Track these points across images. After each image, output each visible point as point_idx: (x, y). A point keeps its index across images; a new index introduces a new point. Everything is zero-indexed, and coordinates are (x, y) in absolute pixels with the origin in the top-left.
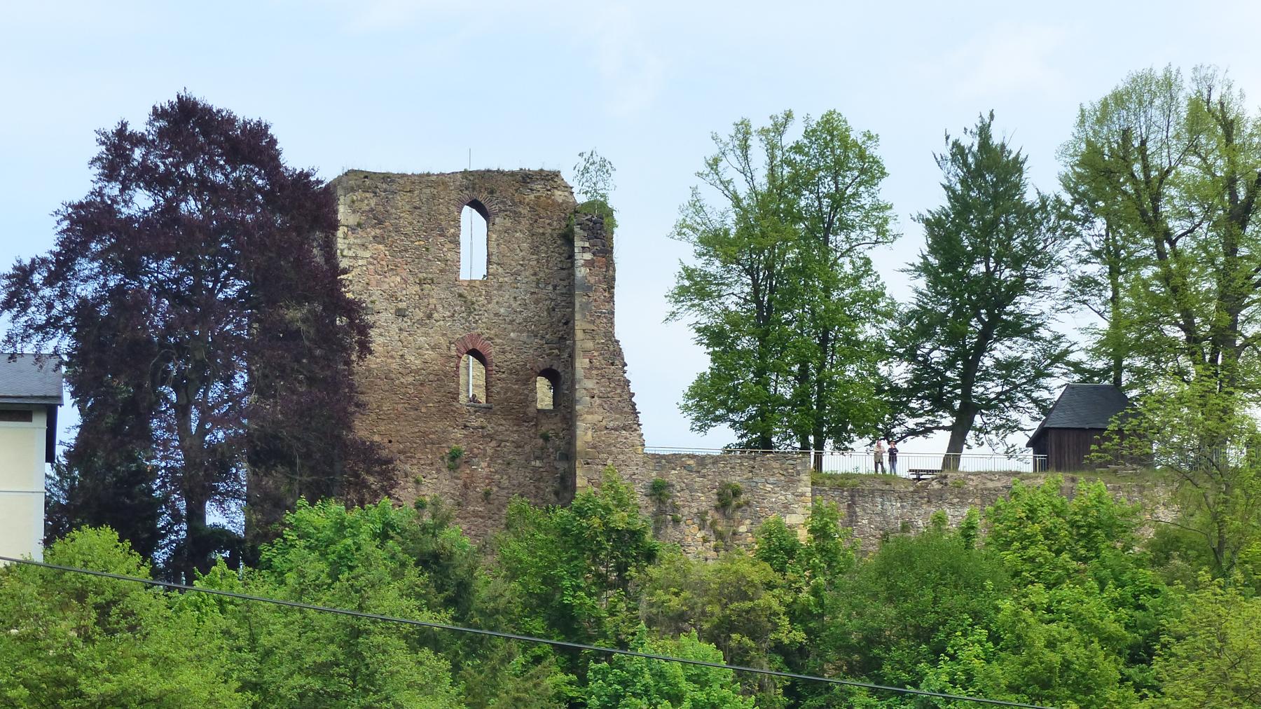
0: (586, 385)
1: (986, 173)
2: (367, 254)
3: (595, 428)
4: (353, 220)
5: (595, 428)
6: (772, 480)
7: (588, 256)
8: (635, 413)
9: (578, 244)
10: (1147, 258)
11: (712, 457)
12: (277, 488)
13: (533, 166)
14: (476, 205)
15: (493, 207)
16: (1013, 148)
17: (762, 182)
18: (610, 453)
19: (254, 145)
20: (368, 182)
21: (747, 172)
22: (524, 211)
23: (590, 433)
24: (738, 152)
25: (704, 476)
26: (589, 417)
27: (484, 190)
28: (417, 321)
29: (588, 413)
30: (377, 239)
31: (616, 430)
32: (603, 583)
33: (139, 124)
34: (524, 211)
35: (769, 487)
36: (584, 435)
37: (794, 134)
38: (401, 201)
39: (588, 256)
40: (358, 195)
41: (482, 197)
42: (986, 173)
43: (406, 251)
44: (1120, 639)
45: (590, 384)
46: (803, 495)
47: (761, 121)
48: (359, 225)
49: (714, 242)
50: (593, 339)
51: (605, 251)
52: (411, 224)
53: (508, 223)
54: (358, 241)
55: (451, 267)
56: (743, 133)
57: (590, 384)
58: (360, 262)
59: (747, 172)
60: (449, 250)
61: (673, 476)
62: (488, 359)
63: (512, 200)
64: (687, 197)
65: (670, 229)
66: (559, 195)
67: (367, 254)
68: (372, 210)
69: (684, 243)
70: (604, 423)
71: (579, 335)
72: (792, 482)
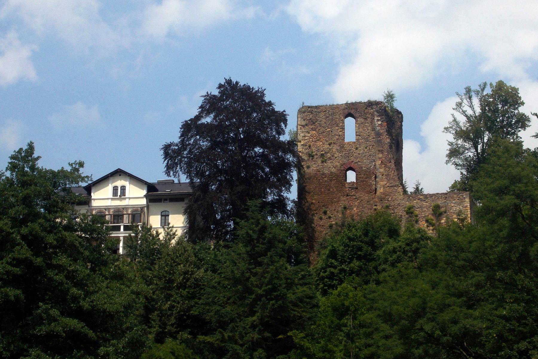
2: (309, 135)
3: (384, 187)
5: (384, 187)
6: (454, 202)
7: (380, 123)
9: (376, 118)
11: (430, 195)
12: (165, 216)
15: (357, 115)
17: (478, 110)
18: (390, 196)
20: (309, 109)
21: (471, 106)
23: (382, 189)
24: (468, 100)
25: (427, 202)
26: (382, 183)
29: (381, 181)
31: (392, 187)
33: (216, 92)
35: (453, 205)
37: (488, 91)
38: (322, 115)
39: (380, 123)
43: (324, 133)
46: (466, 207)
47: (475, 87)
48: (306, 125)
49: (461, 134)
50: (382, 153)
52: (325, 123)
53: (363, 120)
54: (306, 130)
55: (342, 137)
56: (468, 91)
58: (306, 138)
59: (471, 106)
60: (340, 131)
61: (440, 202)
62: (354, 168)
63: (364, 112)
64: (452, 119)
67: (309, 135)
68: (310, 119)
69: (448, 134)
70: (388, 185)
72: (462, 202)
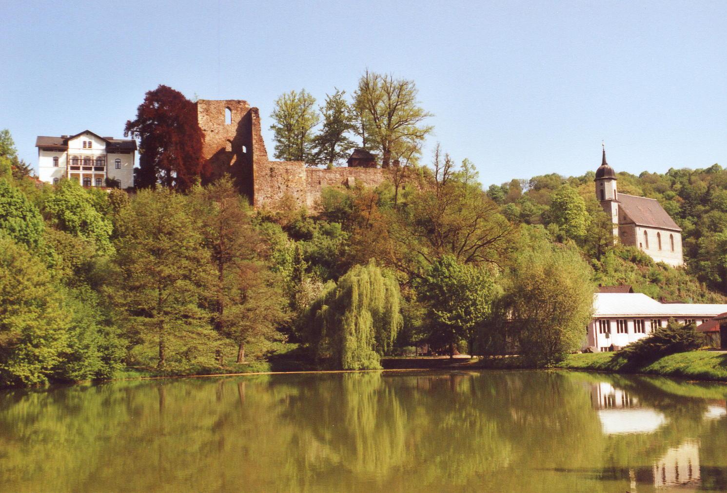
0: (255, 146)
1: (336, 104)
4: (201, 110)
8: (266, 152)
10: (418, 333)
13: (236, 98)
14: (228, 108)
15: (232, 108)
16: (144, 97)
19: (177, 96)
22: (239, 109)
27: (231, 105)
28: (217, 132)
30: (207, 115)
32: (205, 225)
34: (239, 109)
36: (255, 158)
38: (212, 107)
40: (202, 105)
41: (230, 106)
42: (336, 104)
44: (390, 339)
45: (256, 146)
51: (258, 117)
53: (235, 111)
55: (224, 121)
57: (256, 146)
65: (269, 115)
66: (247, 106)
71: (253, 135)
